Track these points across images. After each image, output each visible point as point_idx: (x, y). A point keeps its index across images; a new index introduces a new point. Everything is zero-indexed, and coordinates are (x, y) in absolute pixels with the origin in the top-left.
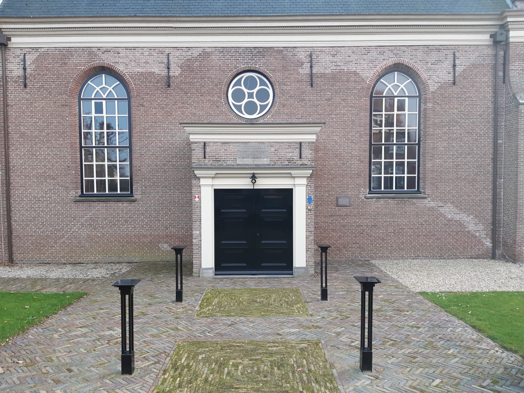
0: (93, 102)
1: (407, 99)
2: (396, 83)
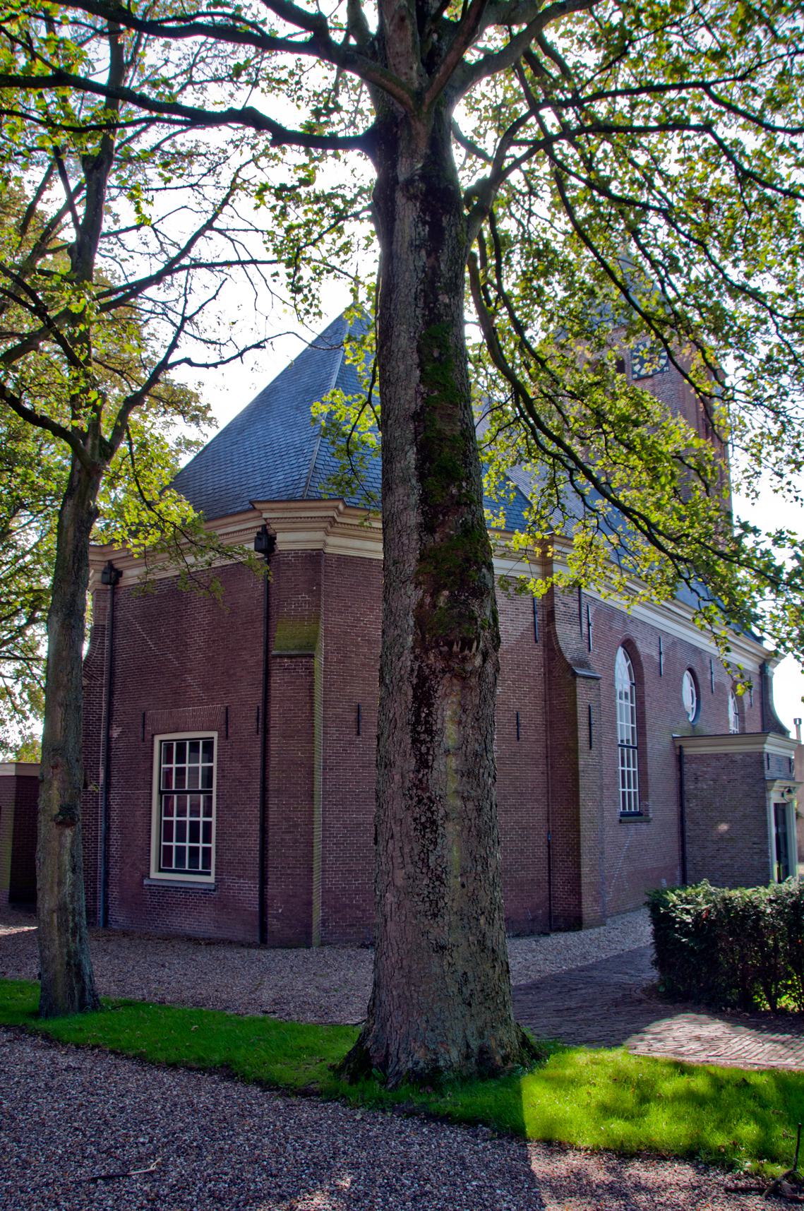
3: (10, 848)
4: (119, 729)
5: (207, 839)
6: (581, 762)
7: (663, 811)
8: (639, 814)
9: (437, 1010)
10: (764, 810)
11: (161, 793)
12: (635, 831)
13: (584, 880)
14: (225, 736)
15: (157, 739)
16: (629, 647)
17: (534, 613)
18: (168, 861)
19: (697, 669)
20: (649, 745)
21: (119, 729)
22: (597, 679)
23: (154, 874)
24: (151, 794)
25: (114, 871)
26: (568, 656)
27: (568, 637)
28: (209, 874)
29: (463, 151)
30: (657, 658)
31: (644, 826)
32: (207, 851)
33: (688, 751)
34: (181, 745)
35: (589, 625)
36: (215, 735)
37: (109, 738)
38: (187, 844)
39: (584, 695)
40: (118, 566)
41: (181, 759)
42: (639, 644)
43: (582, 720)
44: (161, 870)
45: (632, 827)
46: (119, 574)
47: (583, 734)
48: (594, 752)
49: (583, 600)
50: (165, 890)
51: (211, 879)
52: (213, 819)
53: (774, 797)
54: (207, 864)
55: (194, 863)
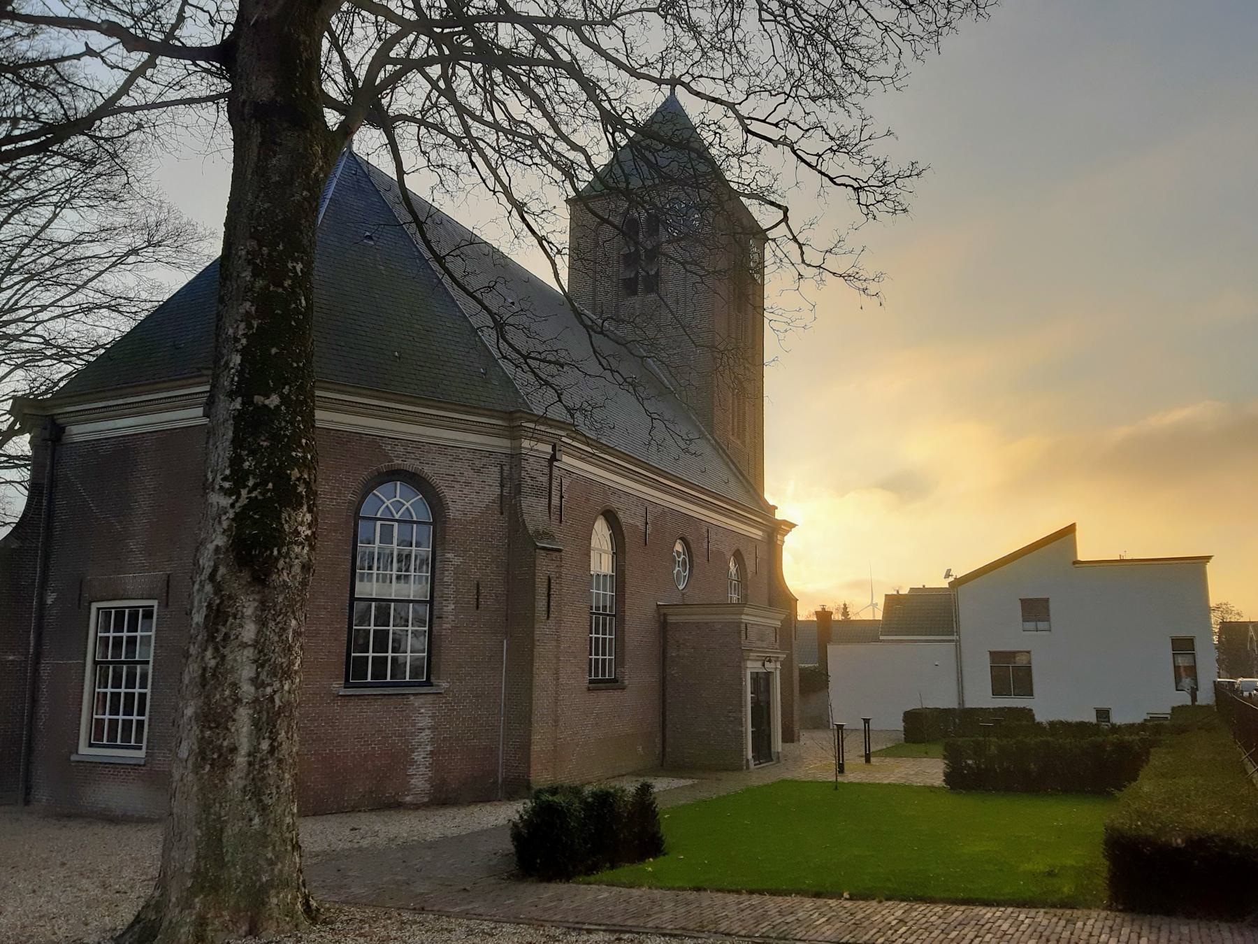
0: (379, 523)
1: (396, 524)
2: (398, 498)
3: (1070, 720)
4: (54, 595)
5: (141, 712)
6: (537, 632)
7: (639, 678)
8: (615, 681)
9: (704, 904)
10: (740, 680)
11: (95, 663)
12: (604, 699)
13: (534, 748)
14: (165, 604)
15: (94, 606)
16: (611, 517)
17: (502, 486)
18: (99, 736)
19: (690, 538)
20: (628, 613)
21: (54, 595)
22: (560, 551)
23: (83, 749)
24: (84, 665)
25: (668, 750)
26: (531, 529)
27: (534, 511)
28: (140, 748)
29: (124, 98)
30: (642, 528)
31: (617, 693)
32: (140, 724)
33: (671, 619)
34: (120, 613)
35: (562, 497)
36: (155, 603)
37: (42, 602)
38: (107, 717)
39: (544, 568)
40: (61, 421)
41: (133, 628)
42: (621, 515)
43: (541, 589)
44: (91, 745)
45: (603, 696)
46: (61, 430)
47: (541, 605)
48: (551, 622)
49: (556, 472)
50: (93, 766)
51: (141, 754)
52: (148, 691)
53: (753, 666)
54: (139, 739)
55: (126, 738)
